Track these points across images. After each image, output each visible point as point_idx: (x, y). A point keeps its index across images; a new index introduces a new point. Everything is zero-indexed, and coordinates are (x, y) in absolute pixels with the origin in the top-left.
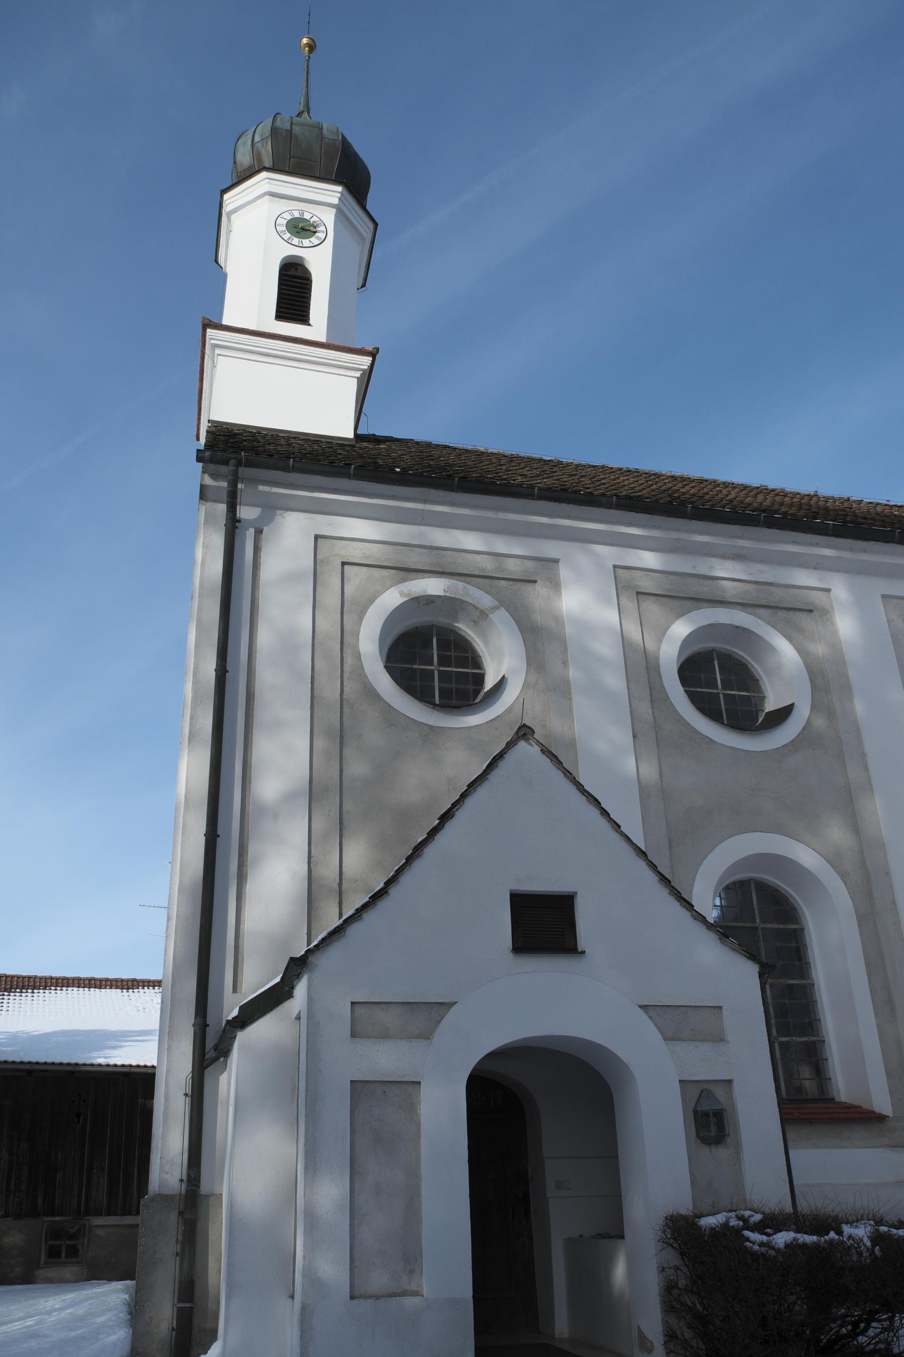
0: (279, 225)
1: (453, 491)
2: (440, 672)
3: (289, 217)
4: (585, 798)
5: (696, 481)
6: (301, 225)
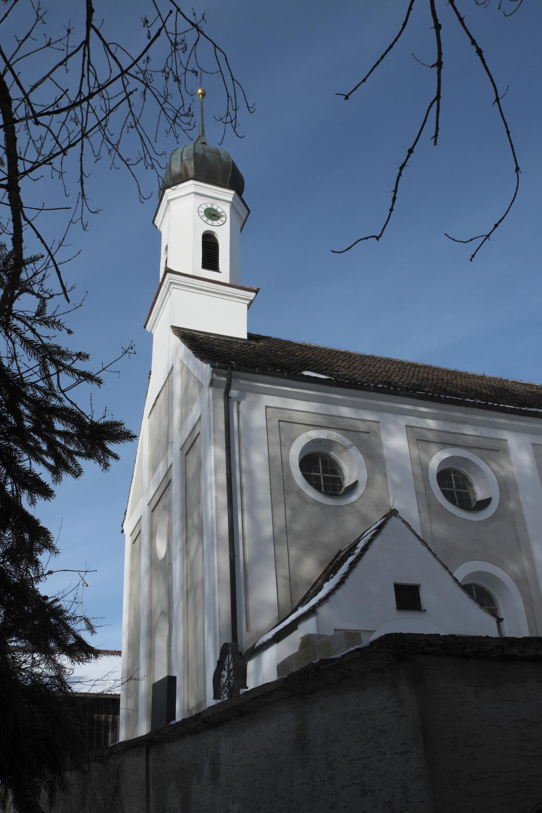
0: (200, 212)
1: (332, 386)
2: (324, 477)
3: (205, 208)
4: (421, 543)
5: (422, 367)
6: (212, 213)
